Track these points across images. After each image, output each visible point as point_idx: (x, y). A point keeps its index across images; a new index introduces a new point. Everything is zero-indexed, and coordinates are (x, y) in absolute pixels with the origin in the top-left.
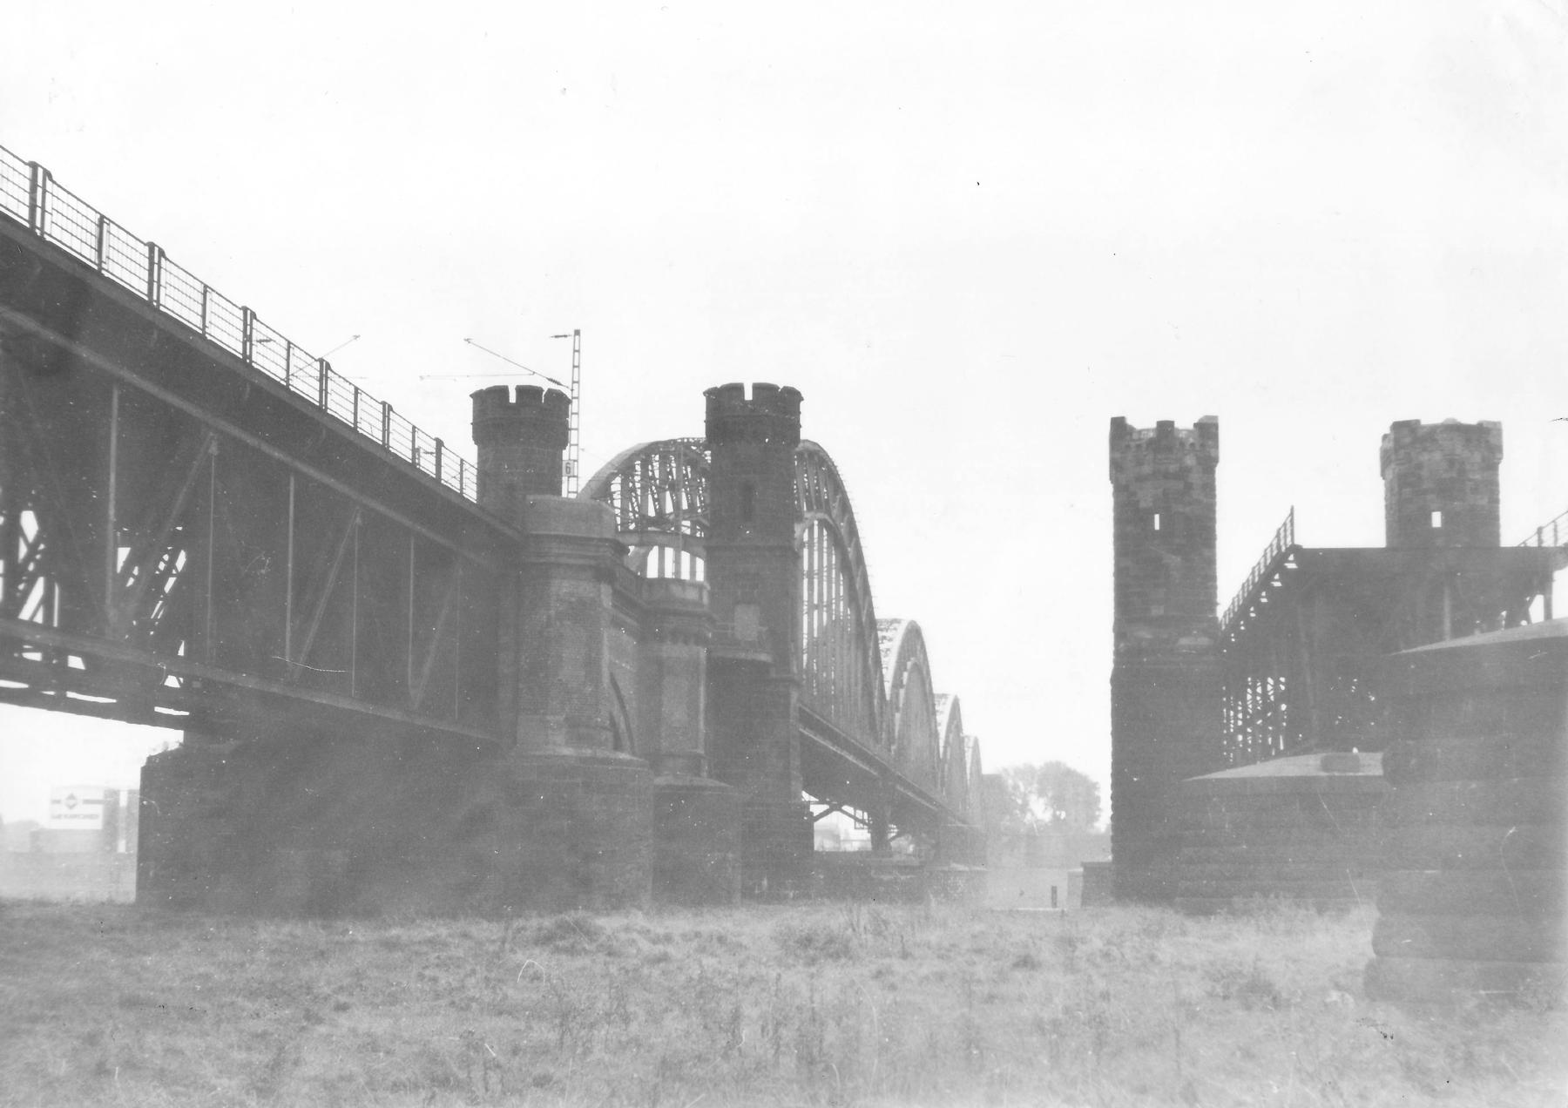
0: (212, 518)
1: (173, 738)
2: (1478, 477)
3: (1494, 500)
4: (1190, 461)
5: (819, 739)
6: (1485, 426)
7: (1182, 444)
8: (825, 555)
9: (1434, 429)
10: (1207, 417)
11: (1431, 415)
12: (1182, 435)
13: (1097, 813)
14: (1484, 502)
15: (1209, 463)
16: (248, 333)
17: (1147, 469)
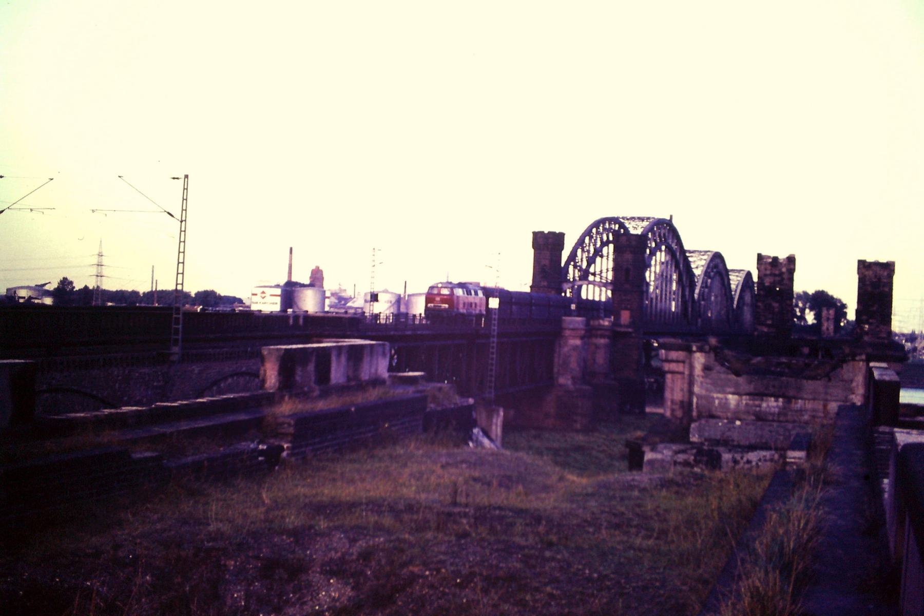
0: (180, 335)
2: (885, 281)
4: (784, 270)
5: (230, 418)
7: (781, 263)
8: (669, 267)
10: (790, 255)
11: (870, 259)
12: (781, 261)
13: (845, 310)
14: (887, 289)
15: (791, 271)
17: (768, 272)
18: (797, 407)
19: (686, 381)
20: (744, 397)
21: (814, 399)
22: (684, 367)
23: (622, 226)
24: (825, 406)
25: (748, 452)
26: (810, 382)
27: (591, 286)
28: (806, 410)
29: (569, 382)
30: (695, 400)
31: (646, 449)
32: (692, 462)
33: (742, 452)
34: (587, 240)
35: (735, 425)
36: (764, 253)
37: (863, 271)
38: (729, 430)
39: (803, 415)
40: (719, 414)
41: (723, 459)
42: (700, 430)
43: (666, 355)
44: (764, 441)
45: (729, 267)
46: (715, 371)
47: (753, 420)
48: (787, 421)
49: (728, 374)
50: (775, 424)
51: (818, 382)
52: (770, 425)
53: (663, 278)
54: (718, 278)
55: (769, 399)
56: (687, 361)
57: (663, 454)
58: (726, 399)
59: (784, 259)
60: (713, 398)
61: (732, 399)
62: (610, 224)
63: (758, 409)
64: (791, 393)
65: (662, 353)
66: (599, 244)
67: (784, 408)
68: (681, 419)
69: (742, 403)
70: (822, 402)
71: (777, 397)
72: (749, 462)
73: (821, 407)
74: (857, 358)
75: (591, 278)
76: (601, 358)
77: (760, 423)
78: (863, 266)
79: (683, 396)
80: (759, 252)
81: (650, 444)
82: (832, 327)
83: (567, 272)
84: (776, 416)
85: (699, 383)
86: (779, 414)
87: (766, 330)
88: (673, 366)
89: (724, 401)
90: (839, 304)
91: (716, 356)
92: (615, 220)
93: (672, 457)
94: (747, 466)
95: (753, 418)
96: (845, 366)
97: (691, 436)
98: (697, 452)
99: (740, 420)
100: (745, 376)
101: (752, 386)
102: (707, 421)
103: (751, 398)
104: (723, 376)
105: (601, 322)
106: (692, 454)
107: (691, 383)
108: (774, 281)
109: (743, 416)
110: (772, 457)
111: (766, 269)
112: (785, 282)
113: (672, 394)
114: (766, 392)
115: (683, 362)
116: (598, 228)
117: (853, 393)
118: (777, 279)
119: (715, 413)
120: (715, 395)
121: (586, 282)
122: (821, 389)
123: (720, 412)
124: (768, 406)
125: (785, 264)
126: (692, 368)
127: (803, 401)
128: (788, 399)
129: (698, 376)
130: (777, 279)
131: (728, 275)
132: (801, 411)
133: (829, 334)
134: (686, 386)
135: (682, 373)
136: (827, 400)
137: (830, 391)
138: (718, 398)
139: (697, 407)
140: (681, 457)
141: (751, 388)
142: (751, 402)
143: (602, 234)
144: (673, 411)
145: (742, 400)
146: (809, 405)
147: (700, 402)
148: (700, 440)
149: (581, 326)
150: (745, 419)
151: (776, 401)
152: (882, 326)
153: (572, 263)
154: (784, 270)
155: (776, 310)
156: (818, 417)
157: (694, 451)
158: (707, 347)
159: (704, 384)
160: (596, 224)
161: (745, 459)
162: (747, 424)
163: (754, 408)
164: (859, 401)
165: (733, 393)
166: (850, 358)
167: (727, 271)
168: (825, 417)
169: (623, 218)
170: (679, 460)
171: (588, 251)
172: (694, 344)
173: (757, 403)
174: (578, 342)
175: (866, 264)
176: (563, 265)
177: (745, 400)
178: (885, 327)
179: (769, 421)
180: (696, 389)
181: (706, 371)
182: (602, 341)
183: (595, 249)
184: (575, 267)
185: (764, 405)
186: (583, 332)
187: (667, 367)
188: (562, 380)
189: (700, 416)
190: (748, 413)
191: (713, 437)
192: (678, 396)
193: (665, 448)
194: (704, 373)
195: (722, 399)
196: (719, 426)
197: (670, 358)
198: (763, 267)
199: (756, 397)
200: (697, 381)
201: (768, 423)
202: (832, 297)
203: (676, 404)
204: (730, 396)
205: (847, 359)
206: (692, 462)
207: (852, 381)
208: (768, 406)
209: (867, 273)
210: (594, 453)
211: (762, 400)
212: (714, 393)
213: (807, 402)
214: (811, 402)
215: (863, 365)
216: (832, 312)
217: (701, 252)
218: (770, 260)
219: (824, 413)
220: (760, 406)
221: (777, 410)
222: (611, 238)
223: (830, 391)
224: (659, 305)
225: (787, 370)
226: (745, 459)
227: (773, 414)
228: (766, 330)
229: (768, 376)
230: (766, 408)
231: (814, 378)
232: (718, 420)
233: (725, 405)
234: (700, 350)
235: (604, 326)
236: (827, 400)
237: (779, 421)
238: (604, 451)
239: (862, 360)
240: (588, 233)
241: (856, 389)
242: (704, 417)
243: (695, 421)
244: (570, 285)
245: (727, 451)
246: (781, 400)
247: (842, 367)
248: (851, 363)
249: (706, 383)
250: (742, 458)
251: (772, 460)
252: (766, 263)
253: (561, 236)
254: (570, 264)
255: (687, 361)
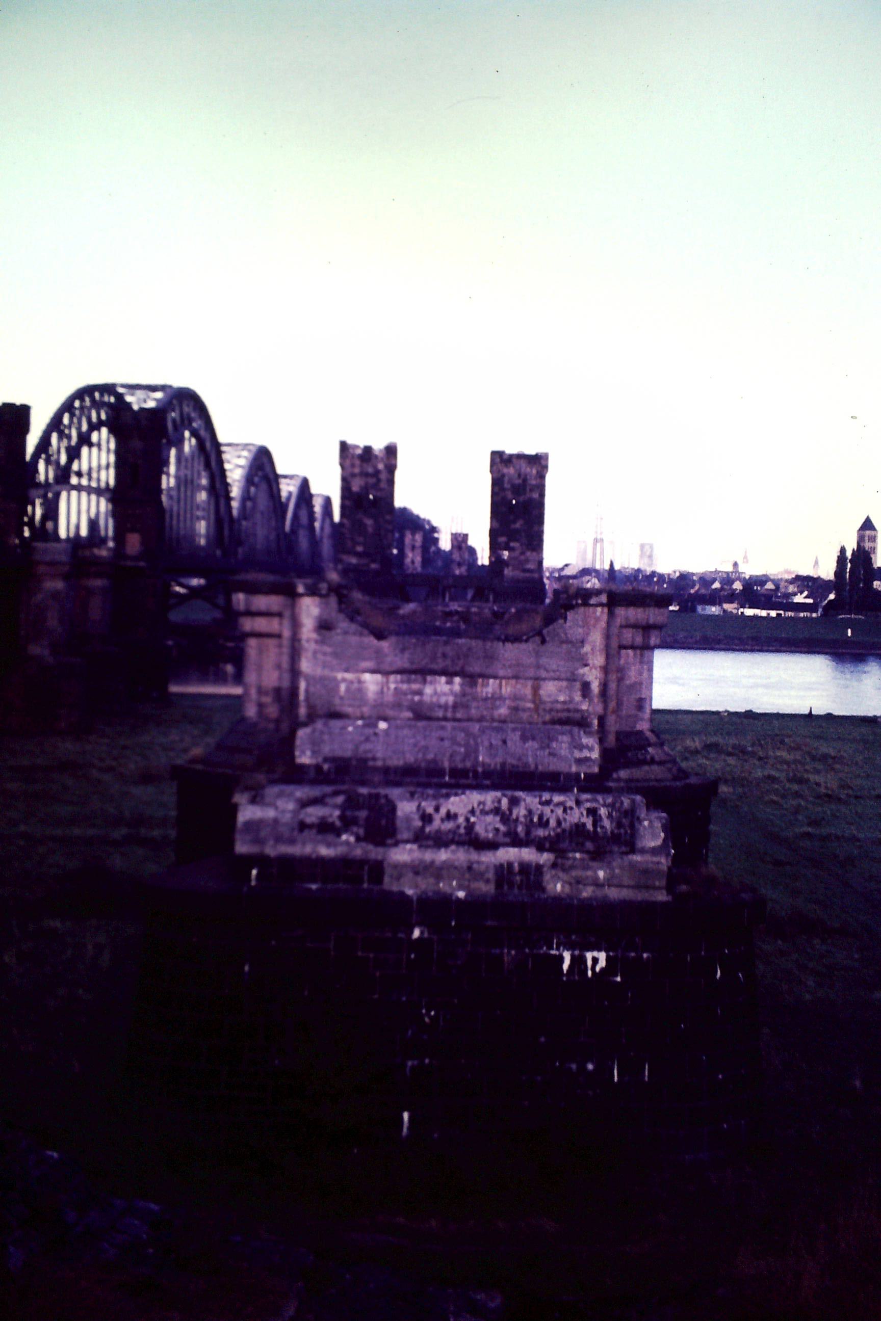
1: (484, 558)
3: (542, 495)
4: (381, 466)
6: (37, 475)
7: (376, 457)
9: (511, 456)
10: (391, 443)
11: (511, 449)
13: (436, 535)
14: (535, 495)
16: (613, 677)
18: (487, 693)
19: (286, 650)
20: (392, 678)
21: (516, 677)
22: (281, 624)
23: (120, 397)
24: (536, 690)
25: (448, 796)
26: (508, 645)
27: (74, 494)
28: (501, 698)
29: (46, 652)
30: (303, 685)
31: (240, 798)
32: (338, 823)
33: (435, 797)
34: (66, 420)
35: (377, 731)
36: (350, 441)
37: (500, 466)
38: (367, 739)
39: (498, 708)
40: (349, 710)
41: (399, 813)
42: (315, 745)
43: (247, 603)
44: (430, 756)
45: (280, 470)
46: (339, 631)
47: (409, 719)
48: (469, 720)
49: (361, 634)
50: (449, 725)
51: (523, 646)
52: (443, 728)
53: (186, 483)
54: (264, 486)
55: (438, 678)
56: (287, 614)
57: (276, 808)
58: (360, 682)
59: (381, 450)
60: (335, 679)
61: (371, 682)
62: (102, 395)
63: (417, 698)
64: (475, 667)
65: (239, 600)
66: (85, 427)
67: (464, 694)
68: (277, 721)
69: (388, 688)
70: (530, 683)
71: (449, 674)
72: (450, 816)
73: (528, 691)
74: (593, 601)
75: (74, 480)
76: (96, 609)
77: (421, 724)
78: (499, 459)
79: (280, 678)
80: (343, 439)
81: (247, 788)
82: (418, 559)
83: (36, 471)
84: (450, 710)
85: (310, 654)
86: (455, 706)
87: (354, 561)
88: (261, 624)
89: (356, 685)
90: (427, 527)
91: (340, 602)
92: (108, 389)
93: (295, 813)
94: (449, 825)
95: (409, 714)
96: (570, 615)
97: (297, 753)
98: (346, 801)
99: (385, 719)
100: (393, 639)
101: (407, 655)
102: (325, 724)
103: (405, 677)
104: (354, 640)
105: (96, 551)
106: (336, 806)
107: (295, 653)
108: (367, 484)
109: (390, 713)
110: (496, 805)
111: (353, 466)
112: (383, 485)
113: (259, 675)
114: (434, 666)
115: (280, 615)
116: (82, 400)
117: (586, 665)
118: (372, 481)
119: (338, 708)
120: (340, 676)
121: (68, 487)
122: (529, 660)
123: (350, 706)
124: (436, 693)
125: (382, 459)
126: (296, 625)
127: (498, 681)
128: (471, 679)
129: (308, 641)
130: (372, 481)
131: (278, 484)
132: (496, 698)
133: (415, 569)
134: (285, 662)
135: (279, 636)
136: (537, 679)
137: (543, 661)
138: (344, 680)
139: (307, 699)
140: (313, 814)
141: (402, 661)
142: (405, 687)
143: (89, 410)
144: (261, 706)
145: (387, 682)
146: (507, 689)
147: (312, 689)
148: (314, 762)
149: (64, 558)
150: (395, 719)
151: (449, 682)
152: (528, 553)
153: (43, 456)
154: (381, 466)
155: (370, 530)
156: (524, 710)
157: (340, 799)
158: (324, 586)
159: (319, 656)
160: (81, 394)
161: (443, 811)
162: (397, 727)
163: (409, 697)
164: (596, 678)
165: (373, 671)
166: (580, 602)
167: (277, 477)
168: (536, 709)
169: (123, 386)
170: (309, 820)
171: (69, 437)
172: (302, 580)
173: (415, 686)
174: (59, 585)
175: (505, 457)
176: (28, 457)
177: (394, 682)
178: (534, 554)
179: (438, 719)
180: (305, 665)
181: (324, 632)
182: (98, 583)
183: (80, 435)
184: (48, 462)
185: (428, 690)
186: (67, 568)
187: (248, 624)
188: (35, 650)
189: (312, 718)
190: (398, 706)
191: (339, 753)
192: (271, 678)
193: (280, 795)
194: (319, 634)
195: (352, 682)
196: (350, 733)
197: (254, 608)
198: (348, 462)
199: (413, 677)
200: (306, 650)
201: (435, 724)
202: (418, 517)
203: (266, 693)
204: (367, 677)
205: (574, 602)
206: (338, 823)
207: (582, 642)
208: (436, 693)
209: (505, 471)
210: (95, 773)
211: (425, 682)
212: (338, 671)
213: (504, 682)
214: (513, 682)
215: (602, 612)
216: (419, 537)
217: (237, 445)
218: (359, 452)
219: (534, 702)
220: (420, 693)
221: (451, 699)
222: (103, 416)
223: (543, 661)
224: (182, 525)
225: (463, 626)
226: (443, 811)
227: (445, 707)
228: (354, 561)
229: (434, 638)
230: (431, 696)
231: (516, 639)
232: (347, 721)
233: (359, 692)
234: (312, 591)
235: (100, 557)
236: (537, 679)
237: (455, 720)
238: (110, 769)
239: (601, 605)
240: (67, 407)
241: (590, 656)
242: (320, 717)
243: (305, 725)
244: (41, 492)
245: (408, 795)
246: (457, 680)
247: (565, 618)
248: (582, 610)
249: (325, 654)
250: (437, 809)
251: (497, 811)
252: (353, 456)
253: (24, 411)
254: (40, 457)
255: (287, 614)
